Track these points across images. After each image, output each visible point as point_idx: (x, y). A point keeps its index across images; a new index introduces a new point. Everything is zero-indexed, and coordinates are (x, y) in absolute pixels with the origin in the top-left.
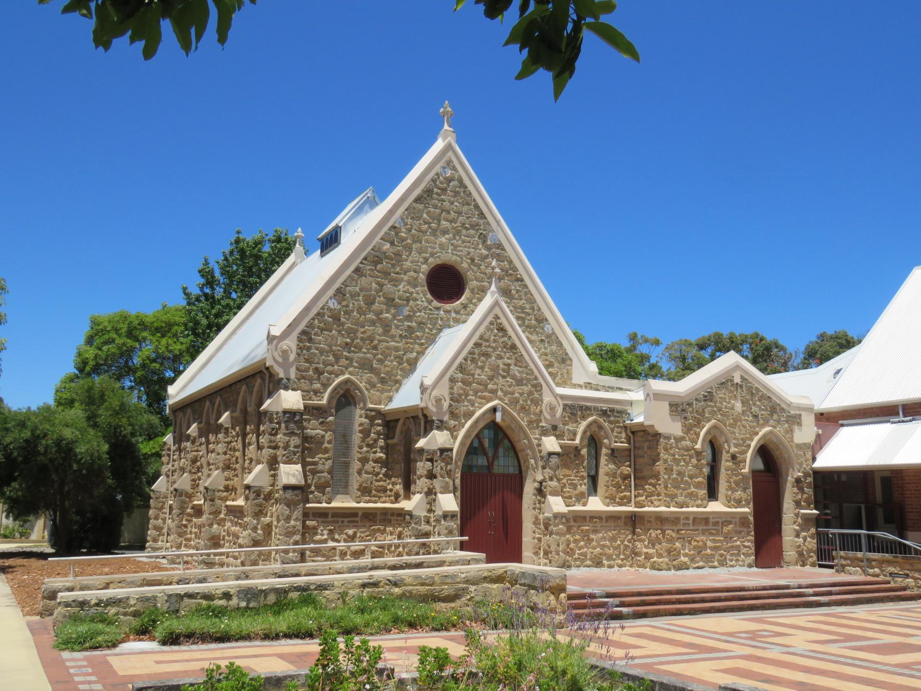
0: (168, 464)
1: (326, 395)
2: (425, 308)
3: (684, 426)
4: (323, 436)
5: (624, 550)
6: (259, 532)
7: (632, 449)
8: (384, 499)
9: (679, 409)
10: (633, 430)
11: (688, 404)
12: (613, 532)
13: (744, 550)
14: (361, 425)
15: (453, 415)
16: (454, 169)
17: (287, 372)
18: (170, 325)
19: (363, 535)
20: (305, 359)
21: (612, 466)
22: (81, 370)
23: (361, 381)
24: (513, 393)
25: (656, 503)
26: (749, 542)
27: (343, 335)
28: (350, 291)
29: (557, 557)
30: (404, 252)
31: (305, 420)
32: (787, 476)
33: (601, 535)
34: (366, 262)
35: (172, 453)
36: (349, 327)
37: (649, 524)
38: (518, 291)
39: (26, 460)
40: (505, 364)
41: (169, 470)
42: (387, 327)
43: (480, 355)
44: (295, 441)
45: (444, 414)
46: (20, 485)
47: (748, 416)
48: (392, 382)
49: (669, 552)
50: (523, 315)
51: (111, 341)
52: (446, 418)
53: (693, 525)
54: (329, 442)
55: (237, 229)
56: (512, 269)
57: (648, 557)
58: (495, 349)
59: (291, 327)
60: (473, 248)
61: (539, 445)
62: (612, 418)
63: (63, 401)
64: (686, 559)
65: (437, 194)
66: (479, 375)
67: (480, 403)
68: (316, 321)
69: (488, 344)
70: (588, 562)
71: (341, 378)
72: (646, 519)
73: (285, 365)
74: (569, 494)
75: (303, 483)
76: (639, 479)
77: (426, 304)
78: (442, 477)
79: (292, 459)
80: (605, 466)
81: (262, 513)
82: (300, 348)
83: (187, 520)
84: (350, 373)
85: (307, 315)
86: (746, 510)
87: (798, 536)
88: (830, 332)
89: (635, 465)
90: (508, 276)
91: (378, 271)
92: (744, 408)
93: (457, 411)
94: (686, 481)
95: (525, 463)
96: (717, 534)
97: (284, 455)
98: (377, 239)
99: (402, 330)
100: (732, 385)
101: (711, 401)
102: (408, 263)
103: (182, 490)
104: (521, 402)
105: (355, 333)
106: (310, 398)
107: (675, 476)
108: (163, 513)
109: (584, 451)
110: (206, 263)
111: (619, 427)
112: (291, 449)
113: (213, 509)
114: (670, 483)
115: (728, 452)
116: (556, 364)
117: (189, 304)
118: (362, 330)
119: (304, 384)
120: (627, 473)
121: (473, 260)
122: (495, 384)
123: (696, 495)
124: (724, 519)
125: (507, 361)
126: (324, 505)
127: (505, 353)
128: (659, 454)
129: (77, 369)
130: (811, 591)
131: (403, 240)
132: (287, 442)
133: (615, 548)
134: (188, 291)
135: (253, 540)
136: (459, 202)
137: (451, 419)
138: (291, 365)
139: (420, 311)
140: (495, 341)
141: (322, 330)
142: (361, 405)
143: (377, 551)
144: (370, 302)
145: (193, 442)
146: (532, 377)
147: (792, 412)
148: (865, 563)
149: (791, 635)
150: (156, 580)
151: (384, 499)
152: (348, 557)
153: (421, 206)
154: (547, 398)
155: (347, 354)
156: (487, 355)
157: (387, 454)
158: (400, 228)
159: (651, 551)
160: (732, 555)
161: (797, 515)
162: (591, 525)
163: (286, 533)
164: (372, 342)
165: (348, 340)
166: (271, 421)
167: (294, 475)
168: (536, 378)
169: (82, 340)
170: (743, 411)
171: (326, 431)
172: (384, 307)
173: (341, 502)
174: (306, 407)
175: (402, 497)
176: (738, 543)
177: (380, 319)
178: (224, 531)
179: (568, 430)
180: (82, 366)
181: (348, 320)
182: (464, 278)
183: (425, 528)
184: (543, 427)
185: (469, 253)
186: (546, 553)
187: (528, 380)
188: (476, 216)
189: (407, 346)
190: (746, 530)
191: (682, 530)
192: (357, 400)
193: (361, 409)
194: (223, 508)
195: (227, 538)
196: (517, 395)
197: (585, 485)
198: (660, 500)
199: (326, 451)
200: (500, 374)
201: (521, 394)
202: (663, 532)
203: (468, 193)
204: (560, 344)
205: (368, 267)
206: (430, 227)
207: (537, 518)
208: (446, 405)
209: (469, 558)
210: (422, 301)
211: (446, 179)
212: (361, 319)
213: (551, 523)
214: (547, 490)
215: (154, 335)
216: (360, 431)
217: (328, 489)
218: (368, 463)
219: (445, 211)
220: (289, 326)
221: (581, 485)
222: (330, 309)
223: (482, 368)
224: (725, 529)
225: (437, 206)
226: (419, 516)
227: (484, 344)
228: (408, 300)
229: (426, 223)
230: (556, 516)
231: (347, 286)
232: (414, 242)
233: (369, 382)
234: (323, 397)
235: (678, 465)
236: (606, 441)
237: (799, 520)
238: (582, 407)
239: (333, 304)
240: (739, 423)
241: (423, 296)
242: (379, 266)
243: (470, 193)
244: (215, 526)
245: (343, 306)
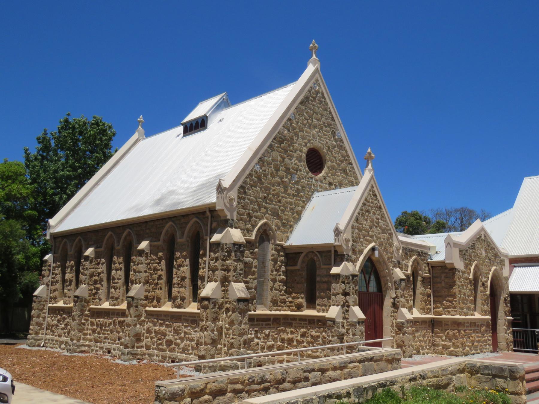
0: (48, 276)
1: (254, 233)
6: (215, 333)
7: (432, 278)
8: (284, 308)
10: (433, 266)
14: (273, 255)
17: (232, 215)
19: (273, 334)
20: (242, 206)
23: (274, 223)
27: (263, 191)
28: (267, 160)
29: (409, 349)
32: (500, 296)
35: (52, 268)
36: (266, 185)
37: (447, 326)
41: (49, 281)
42: (286, 188)
52: (350, 253)
57: (445, 347)
59: (235, 182)
65: (311, 100)
67: (366, 244)
68: (248, 180)
72: (443, 323)
76: (437, 297)
80: (420, 288)
81: (217, 319)
82: (239, 198)
83: (85, 320)
84: (267, 218)
88: (409, 211)
89: (433, 288)
91: (281, 149)
95: (385, 285)
97: (234, 276)
98: (281, 126)
99: (293, 191)
103: (82, 297)
105: (269, 190)
108: (43, 313)
110: (45, 133)
111: (425, 263)
113: (137, 313)
115: (481, 281)
118: (273, 188)
122: (373, 231)
128: (455, 281)
131: (294, 129)
133: (425, 342)
135: (212, 339)
136: (322, 108)
139: (303, 179)
140: (372, 203)
142: (273, 241)
143: (281, 345)
145: (91, 262)
146: (388, 228)
150: (236, 379)
151: (284, 308)
152: (266, 350)
153: (303, 108)
154: (395, 243)
155: (265, 205)
156: (368, 211)
161: (505, 320)
162: (415, 327)
163: (240, 334)
164: (278, 197)
166: (223, 250)
168: (390, 230)
172: (284, 174)
175: (305, 307)
178: (144, 329)
181: (266, 180)
182: (323, 159)
185: (327, 143)
188: (330, 119)
189: (296, 202)
191: (466, 330)
192: (270, 237)
193: (273, 244)
194: (144, 313)
195: (145, 335)
198: (456, 311)
202: (459, 332)
205: (276, 145)
209: (394, 353)
210: (304, 172)
211: (316, 91)
213: (404, 326)
218: (276, 283)
219: (315, 113)
220: (234, 181)
222: (256, 172)
225: (311, 109)
226: (339, 322)
228: (297, 170)
229: (306, 119)
231: (265, 157)
232: (300, 131)
233: (277, 225)
236: (420, 272)
238: (410, 249)
239: (257, 168)
242: (282, 145)
243: (327, 103)
244: (138, 326)
245: (263, 171)
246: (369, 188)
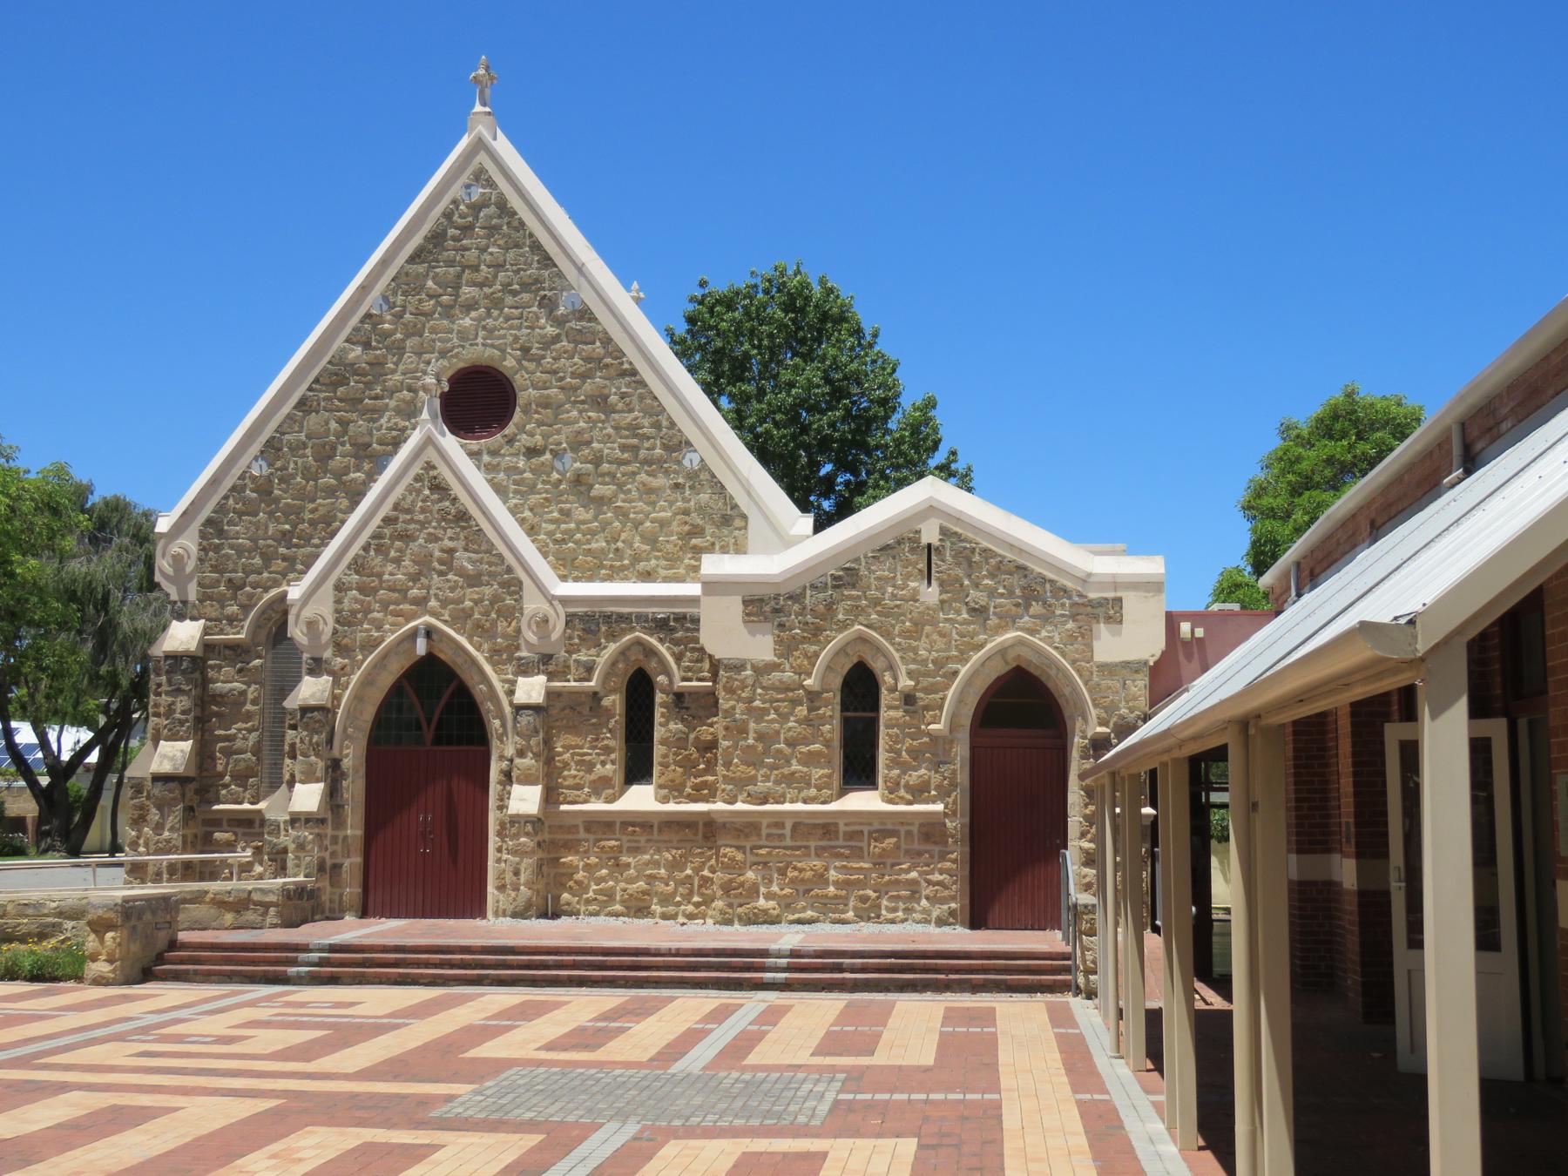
3: (779, 641)
5: (700, 886)
9: (767, 609)
11: (790, 597)
12: (674, 851)
13: (929, 891)
16: (490, 183)
17: (182, 590)
24: (460, 601)
27: (277, 520)
30: (390, 357)
31: (212, 667)
33: (647, 857)
34: (318, 387)
38: (623, 396)
40: (443, 551)
43: (393, 538)
47: (958, 612)
50: (635, 441)
52: (327, 654)
53: (792, 837)
54: (254, 702)
55: (754, 269)
56: (610, 355)
58: (423, 524)
60: (527, 327)
62: (679, 634)
65: (454, 239)
66: (391, 574)
69: (408, 517)
70: (618, 907)
74: (577, 780)
78: (305, 755)
79: (178, 732)
85: (215, 492)
90: (601, 369)
91: (340, 400)
92: (945, 596)
93: (345, 641)
94: (779, 751)
96: (858, 854)
97: (165, 727)
100: (912, 550)
101: (854, 586)
102: (397, 377)
104: (476, 616)
106: (222, 630)
107: (751, 741)
112: (178, 716)
114: (738, 756)
116: (710, 529)
118: (311, 506)
119: (211, 609)
120: (709, 738)
121: (525, 350)
124: (876, 826)
125: (448, 544)
126: (247, 806)
127: (445, 529)
131: (386, 335)
132: (170, 705)
137: (335, 656)
140: (423, 510)
141: (240, 514)
144: (325, 455)
147: (1093, 595)
149: (158, 995)
153: (421, 268)
154: (533, 604)
158: (380, 316)
165: (287, 527)
168: (509, 570)
170: (942, 602)
176: (914, 875)
177: (344, 483)
179: (575, 661)
184: (520, 659)
187: (492, 575)
188: (535, 265)
190: (937, 849)
197: (613, 763)
199: (248, 717)
200: (434, 569)
201: (476, 602)
203: (516, 223)
204: (719, 489)
205: (322, 395)
206: (439, 304)
208: (327, 631)
211: (471, 206)
212: (309, 488)
217: (251, 780)
221: (603, 763)
222: (254, 478)
223: (397, 561)
224: (876, 847)
226: (276, 821)
227: (402, 517)
229: (431, 297)
231: (284, 434)
232: (408, 336)
234: (242, 627)
235: (759, 720)
240: (928, 628)
245: (277, 470)
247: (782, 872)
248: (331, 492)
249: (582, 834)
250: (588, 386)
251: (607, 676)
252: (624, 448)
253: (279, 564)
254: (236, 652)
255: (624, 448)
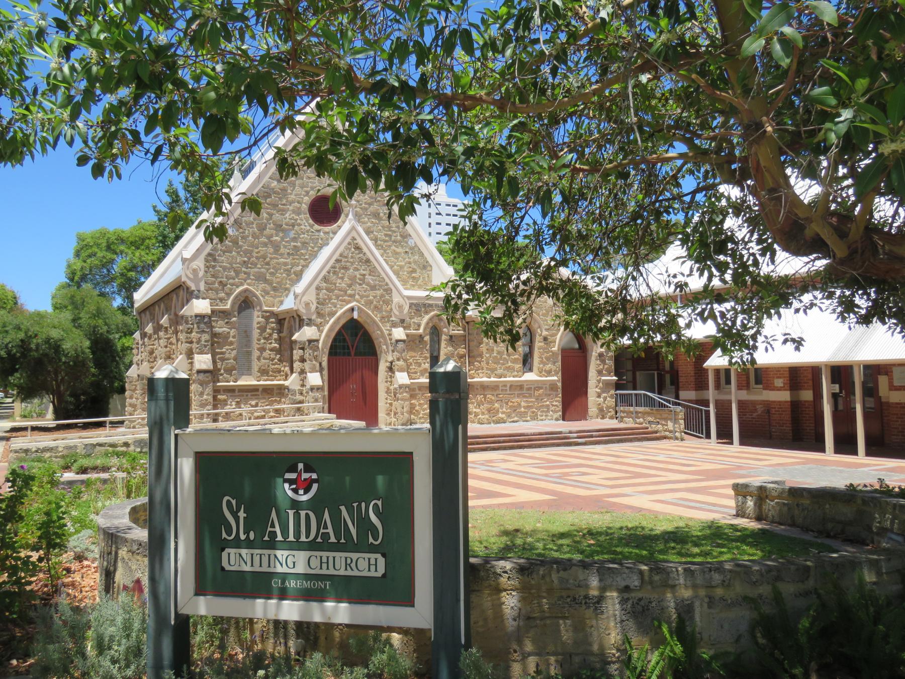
1: (230, 302)
2: (308, 231)
4: (229, 333)
13: (553, 408)
14: (258, 323)
15: (319, 315)
17: (197, 285)
18: (143, 240)
21: (450, 348)
22: (72, 280)
24: (368, 296)
25: (481, 375)
26: (557, 402)
39: (24, 355)
44: (205, 337)
45: (313, 314)
46: (21, 375)
48: (281, 290)
49: (489, 411)
51: (94, 255)
52: (314, 317)
54: (234, 337)
58: (352, 263)
61: (390, 335)
63: (58, 306)
64: (503, 416)
71: (241, 288)
73: (196, 279)
75: (211, 368)
77: (308, 228)
78: (311, 360)
84: (248, 284)
86: (555, 378)
87: (599, 396)
96: (530, 396)
102: (293, 197)
109: (427, 338)
110: (171, 185)
112: (203, 343)
115: (540, 335)
116: (418, 271)
117: (160, 220)
119: (212, 294)
123: (513, 368)
126: (232, 383)
129: (69, 278)
130: (575, 435)
134: (158, 208)
138: (201, 280)
140: (352, 257)
141: (224, 252)
145: (150, 338)
148: (634, 415)
154: (396, 299)
157: (280, 345)
159: (477, 410)
160: (542, 412)
161: (599, 381)
166: (187, 322)
167: (205, 363)
168: (387, 284)
169: (71, 255)
171: (231, 329)
173: (246, 381)
174: (213, 311)
180: (72, 276)
183: (299, 397)
186: (395, 414)
196: (371, 298)
199: (231, 343)
201: (375, 297)
204: (422, 255)
207: (388, 389)
208: (313, 307)
214: (395, 368)
215: (129, 248)
216: (258, 328)
220: (198, 250)
223: (342, 278)
224: (537, 393)
227: (344, 260)
228: (293, 226)
230: (401, 387)
233: (264, 290)
236: (445, 330)
237: (601, 384)
241: (306, 222)
242: (268, 200)
246: (348, 240)
247: (507, 403)
248: (265, 245)
249: (417, 392)
250: (372, 209)
251: (425, 329)
252: (386, 235)
253: (242, 276)
254: (224, 314)
255: (386, 235)
